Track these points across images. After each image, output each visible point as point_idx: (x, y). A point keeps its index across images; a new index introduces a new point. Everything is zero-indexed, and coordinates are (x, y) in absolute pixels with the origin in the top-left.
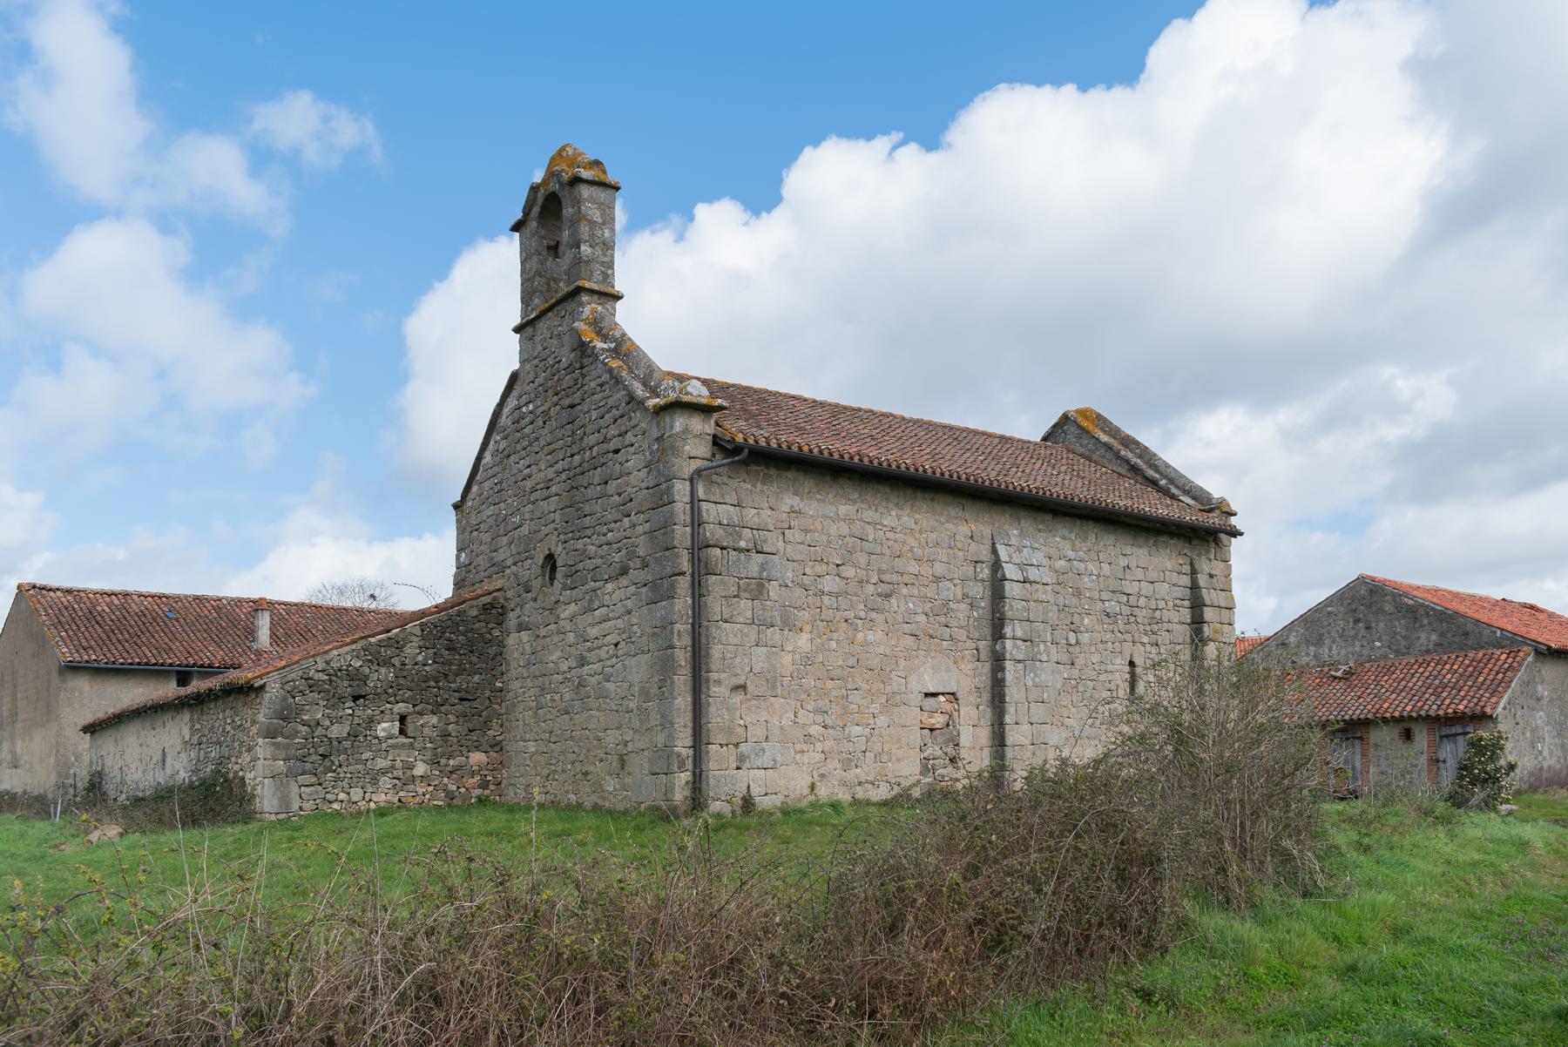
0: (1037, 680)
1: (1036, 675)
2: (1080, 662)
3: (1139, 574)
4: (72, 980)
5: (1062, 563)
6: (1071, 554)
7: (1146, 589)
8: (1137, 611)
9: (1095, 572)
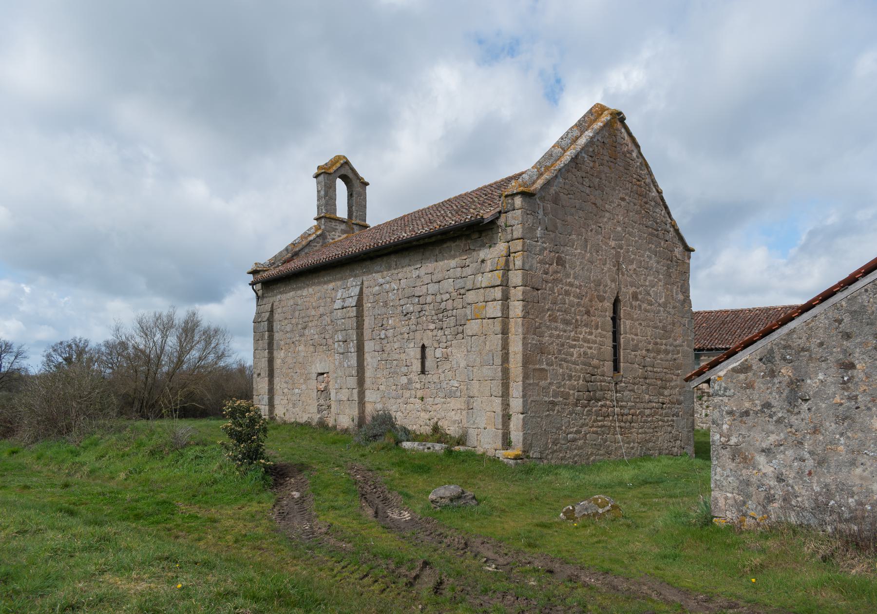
0: (349, 363)
1: (349, 361)
2: (387, 349)
3: (427, 279)
4: (633, 451)
5: (377, 288)
6: (381, 281)
7: (432, 288)
8: (426, 307)
9: (396, 288)
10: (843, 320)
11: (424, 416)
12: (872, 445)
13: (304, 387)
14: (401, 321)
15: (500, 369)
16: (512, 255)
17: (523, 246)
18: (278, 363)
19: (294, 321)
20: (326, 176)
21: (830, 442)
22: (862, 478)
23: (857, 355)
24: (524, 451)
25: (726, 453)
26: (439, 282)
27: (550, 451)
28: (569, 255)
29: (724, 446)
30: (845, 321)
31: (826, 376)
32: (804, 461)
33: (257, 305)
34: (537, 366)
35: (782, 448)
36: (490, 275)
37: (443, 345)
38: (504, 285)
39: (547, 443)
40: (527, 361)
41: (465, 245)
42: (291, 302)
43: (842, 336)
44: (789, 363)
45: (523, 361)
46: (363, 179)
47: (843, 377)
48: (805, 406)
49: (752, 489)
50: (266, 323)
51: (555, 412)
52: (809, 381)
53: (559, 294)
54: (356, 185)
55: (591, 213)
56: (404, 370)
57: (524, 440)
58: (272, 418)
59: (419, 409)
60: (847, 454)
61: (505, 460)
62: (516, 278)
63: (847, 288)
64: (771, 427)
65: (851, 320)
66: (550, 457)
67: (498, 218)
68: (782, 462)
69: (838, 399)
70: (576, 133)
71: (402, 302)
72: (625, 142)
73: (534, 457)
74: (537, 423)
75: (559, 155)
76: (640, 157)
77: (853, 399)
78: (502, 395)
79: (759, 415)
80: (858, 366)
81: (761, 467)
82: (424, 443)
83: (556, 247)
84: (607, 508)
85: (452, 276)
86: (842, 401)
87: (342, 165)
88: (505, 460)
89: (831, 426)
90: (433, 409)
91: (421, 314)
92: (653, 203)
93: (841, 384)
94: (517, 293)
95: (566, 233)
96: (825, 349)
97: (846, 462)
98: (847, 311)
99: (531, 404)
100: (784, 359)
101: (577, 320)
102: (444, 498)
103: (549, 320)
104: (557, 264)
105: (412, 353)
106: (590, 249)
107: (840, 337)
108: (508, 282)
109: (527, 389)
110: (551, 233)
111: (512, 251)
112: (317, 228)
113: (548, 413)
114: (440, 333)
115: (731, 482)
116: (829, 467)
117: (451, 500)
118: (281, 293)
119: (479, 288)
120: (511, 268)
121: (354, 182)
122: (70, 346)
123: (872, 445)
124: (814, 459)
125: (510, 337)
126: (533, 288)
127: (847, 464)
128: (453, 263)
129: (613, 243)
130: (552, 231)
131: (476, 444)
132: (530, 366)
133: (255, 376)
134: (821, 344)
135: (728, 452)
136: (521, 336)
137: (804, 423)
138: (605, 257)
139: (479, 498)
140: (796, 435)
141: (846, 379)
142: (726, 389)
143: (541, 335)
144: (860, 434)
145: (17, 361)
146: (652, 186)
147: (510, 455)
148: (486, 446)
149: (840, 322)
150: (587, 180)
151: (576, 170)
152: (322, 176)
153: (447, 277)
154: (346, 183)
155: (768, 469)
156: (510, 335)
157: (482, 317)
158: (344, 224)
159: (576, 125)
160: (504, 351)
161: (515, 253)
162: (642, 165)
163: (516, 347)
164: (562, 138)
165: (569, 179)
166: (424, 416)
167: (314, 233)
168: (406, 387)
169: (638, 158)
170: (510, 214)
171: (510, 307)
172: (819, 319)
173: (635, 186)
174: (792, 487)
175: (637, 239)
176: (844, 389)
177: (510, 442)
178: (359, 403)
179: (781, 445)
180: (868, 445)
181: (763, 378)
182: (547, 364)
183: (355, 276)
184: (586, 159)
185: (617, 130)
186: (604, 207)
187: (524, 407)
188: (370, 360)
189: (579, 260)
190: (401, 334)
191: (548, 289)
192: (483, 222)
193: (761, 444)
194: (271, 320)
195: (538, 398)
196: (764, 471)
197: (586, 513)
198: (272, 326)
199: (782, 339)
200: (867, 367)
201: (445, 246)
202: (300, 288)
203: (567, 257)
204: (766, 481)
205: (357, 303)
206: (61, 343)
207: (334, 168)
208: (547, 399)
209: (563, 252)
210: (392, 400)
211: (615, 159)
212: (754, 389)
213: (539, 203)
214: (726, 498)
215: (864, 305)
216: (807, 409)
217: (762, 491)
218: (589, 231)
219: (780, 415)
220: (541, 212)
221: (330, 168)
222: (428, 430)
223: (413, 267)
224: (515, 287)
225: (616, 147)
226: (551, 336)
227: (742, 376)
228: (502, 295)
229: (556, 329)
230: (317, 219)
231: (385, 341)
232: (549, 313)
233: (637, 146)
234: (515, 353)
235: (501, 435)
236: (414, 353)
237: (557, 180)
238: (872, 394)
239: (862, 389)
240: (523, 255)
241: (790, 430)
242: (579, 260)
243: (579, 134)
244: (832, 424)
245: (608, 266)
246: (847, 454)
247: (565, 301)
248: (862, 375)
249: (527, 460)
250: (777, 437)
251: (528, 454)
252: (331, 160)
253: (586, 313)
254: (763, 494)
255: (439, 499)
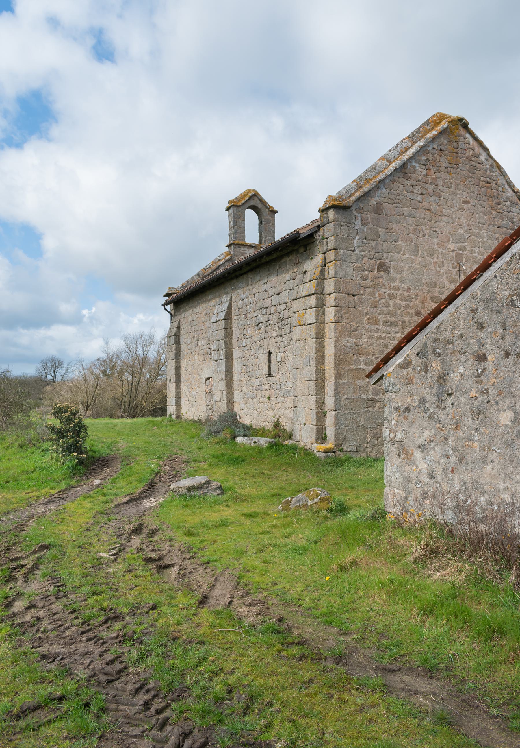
5: (240, 302)
6: (243, 296)
7: (275, 300)
8: (271, 317)
10: (477, 309)
11: (271, 413)
12: (499, 442)
13: (198, 390)
14: (255, 330)
15: (314, 371)
16: (327, 265)
17: (336, 255)
18: (183, 370)
19: (192, 334)
20: (235, 209)
21: (468, 438)
22: (492, 476)
23: (488, 346)
24: (336, 445)
25: (394, 449)
26: (279, 294)
27: (369, 444)
28: (394, 261)
29: (393, 442)
30: (479, 310)
31: (465, 369)
32: (448, 457)
33: (172, 323)
34: (354, 367)
35: (433, 444)
36: (308, 285)
37: (282, 350)
38: (319, 292)
39: (365, 437)
40: (339, 362)
41: (296, 259)
42: (190, 319)
43: (477, 327)
44: (438, 357)
45: (335, 362)
46: (272, 208)
47: (477, 370)
48: (449, 401)
49: (412, 486)
50: (174, 337)
51: (376, 408)
52: (452, 375)
53: (381, 299)
54: (265, 214)
55: (424, 219)
56: (258, 373)
57: (335, 435)
58: (179, 417)
59: (267, 408)
60: (480, 451)
61: (317, 453)
62: (330, 286)
63: (481, 275)
64: (425, 423)
65: (484, 308)
66: (369, 450)
67: (316, 232)
68: (433, 458)
69: (473, 394)
70: (408, 143)
71: (256, 314)
72: (470, 146)
73: (349, 450)
74: (353, 419)
75: (383, 167)
76: (490, 159)
77: (485, 393)
78: (316, 393)
79: (417, 410)
80: (489, 358)
81: (418, 463)
82: (251, 438)
83: (377, 254)
84: (316, 500)
85: (287, 288)
86: (477, 395)
87: (250, 198)
88: (317, 453)
89: (468, 421)
90: (276, 408)
91: (268, 324)
92: (508, 203)
93: (476, 377)
94: (330, 300)
95: (391, 240)
96: (464, 341)
97: (480, 459)
98: (482, 300)
99: (345, 401)
100: (434, 353)
101: (404, 322)
102: (181, 488)
103: (368, 323)
104: (379, 270)
105: (262, 358)
106: (423, 253)
107: (476, 327)
108: (323, 290)
109: (340, 388)
110: (371, 242)
111: (327, 261)
112: (227, 254)
113: (366, 409)
114: (280, 340)
115: (397, 477)
116: (467, 464)
117: (189, 489)
118: (184, 311)
119: (300, 298)
120: (326, 277)
121: (263, 211)
122: (105, 361)
123: (499, 442)
124: (456, 456)
125: (325, 341)
126: (348, 294)
127: (481, 461)
128: (287, 276)
129: (451, 246)
130: (372, 240)
131: (299, 439)
132: (344, 367)
133: (168, 381)
134: (461, 336)
135: (395, 448)
136: (333, 339)
137: (449, 418)
138: (441, 260)
139: (224, 488)
140: (443, 430)
141: (480, 371)
142: (394, 384)
143: (359, 337)
144: (490, 430)
145: (67, 374)
146: (506, 186)
147: (321, 449)
148: (306, 440)
149: (475, 311)
150: (418, 188)
151: (405, 180)
152: (232, 208)
153: (284, 289)
154: (258, 213)
155: (423, 466)
156: (325, 338)
157: (303, 324)
158: (253, 249)
159: (409, 137)
160: (319, 354)
161: (329, 263)
162: (493, 167)
163: (330, 350)
164: (390, 151)
165: (396, 188)
166: (271, 413)
167: (224, 258)
168: (258, 389)
169: (487, 160)
170: (325, 228)
171: (326, 313)
172: (460, 310)
173: (483, 189)
174: (440, 484)
175: (485, 239)
176: (478, 382)
177: (325, 437)
178: (227, 403)
179: (432, 441)
180: (496, 441)
181: (419, 373)
182: (365, 364)
183: (227, 293)
184: (417, 168)
185: (460, 136)
186: (441, 212)
187: (335, 405)
188: (237, 365)
189: (408, 265)
190: (256, 342)
191: (366, 294)
192: (299, 237)
193: (418, 440)
194: (178, 334)
195: (353, 396)
196: (420, 467)
197: (298, 504)
198: (179, 340)
199: (433, 333)
200: (496, 359)
201: (283, 261)
202: (195, 306)
203: (392, 263)
204: (422, 478)
205: (225, 316)
206: (98, 359)
207: (243, 201)
208: (365, 397)
209: (386, 258)
210: (250, 400)
211: (456, 165)
212: (413, 384)
213: (356, 214)
214: (394, 494)
215: (494, 293)
216: (451, 403)
217: (419, 487)
218: (421, 236)
219: (431, 410)
220: (358, 223)
221: (239, 201)
222: (269, 426)
223: (262, 282)
224: (329, 294)
225: (457, 153)
226: (370, 338)
227: (405, 371)
228: (317, 303)
229: (377, 331)
230: (229, 246)
231: (245, 349)
232: (368, 317)
233: (486, 150)
234: (330, 355)
235: (315, 431)
236: (264, 358)
237: (380, 191)
238: (499, 387)
239: (492, 382)
240: (335, 264)
241: (438, 425)
242: (408, 265)
243: (410, 145)
244: (469, 419)
245: (445, 268)
246: (480, 451)
247: (389, 304)
248: (491, 367)
249: (341, 453)
250: (429, 433)
251: (341, 448)
252: (241, 195)
253: (416, 315)
254: (420, 490)
255: (177, 488)
